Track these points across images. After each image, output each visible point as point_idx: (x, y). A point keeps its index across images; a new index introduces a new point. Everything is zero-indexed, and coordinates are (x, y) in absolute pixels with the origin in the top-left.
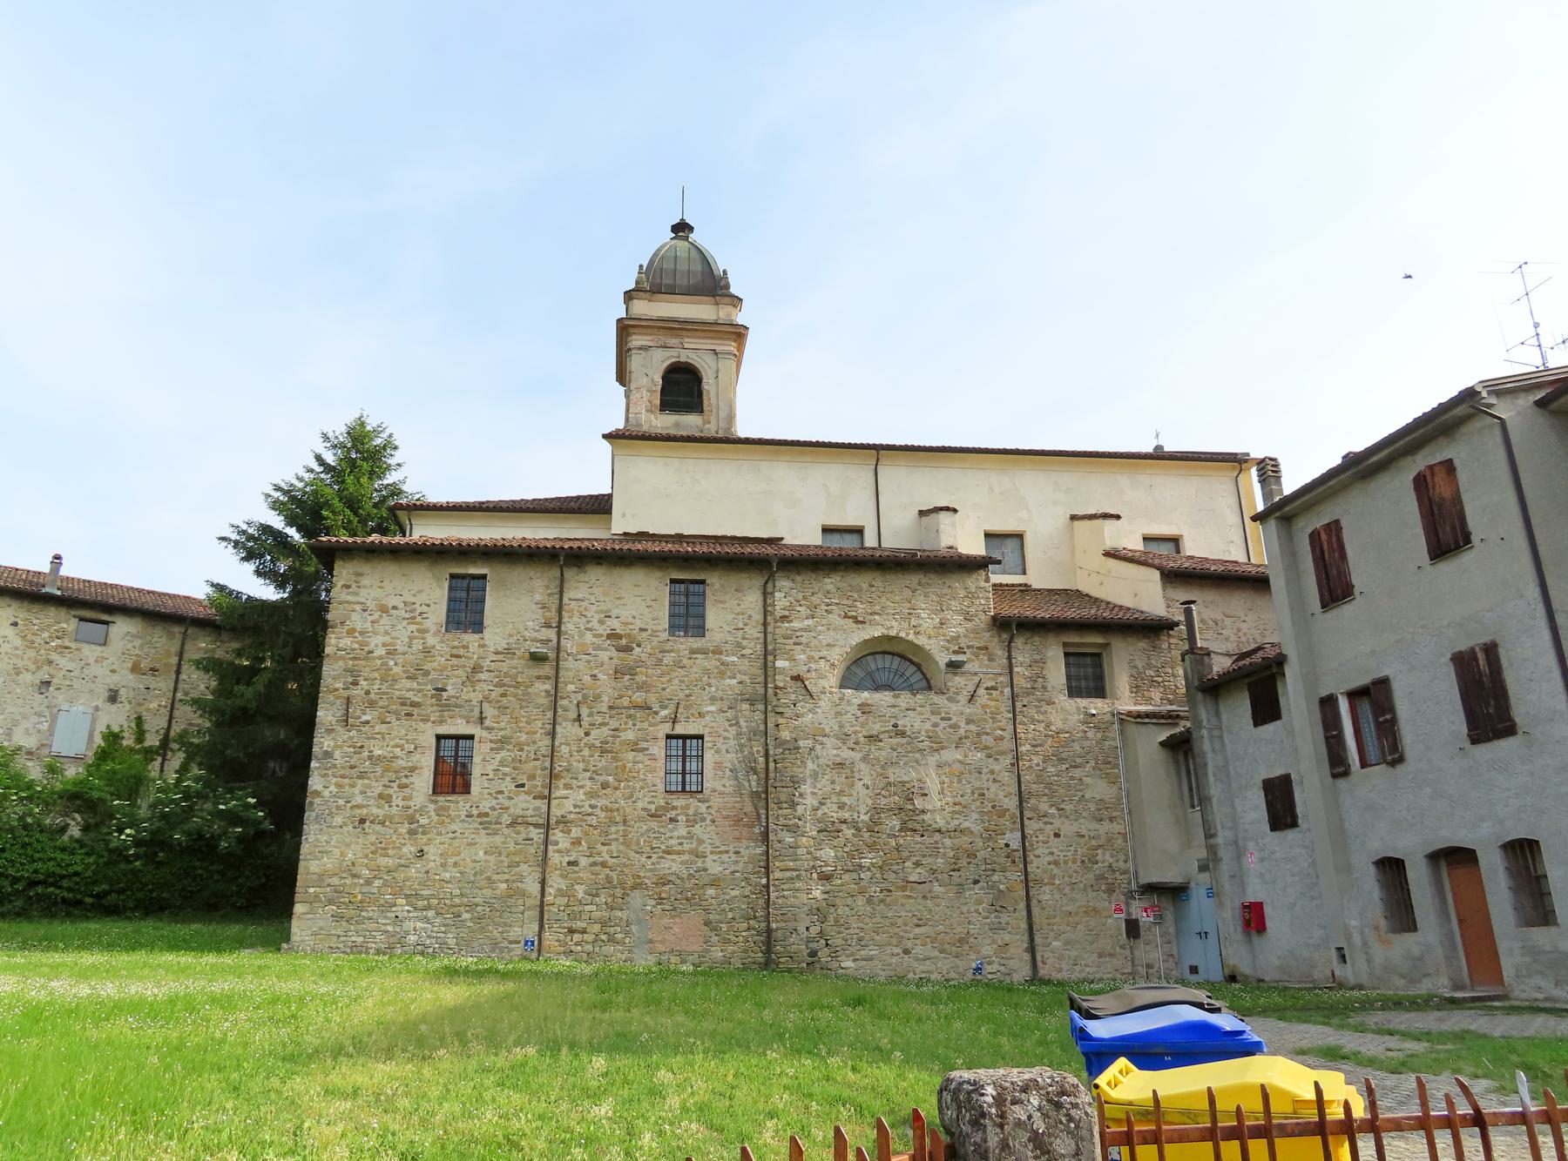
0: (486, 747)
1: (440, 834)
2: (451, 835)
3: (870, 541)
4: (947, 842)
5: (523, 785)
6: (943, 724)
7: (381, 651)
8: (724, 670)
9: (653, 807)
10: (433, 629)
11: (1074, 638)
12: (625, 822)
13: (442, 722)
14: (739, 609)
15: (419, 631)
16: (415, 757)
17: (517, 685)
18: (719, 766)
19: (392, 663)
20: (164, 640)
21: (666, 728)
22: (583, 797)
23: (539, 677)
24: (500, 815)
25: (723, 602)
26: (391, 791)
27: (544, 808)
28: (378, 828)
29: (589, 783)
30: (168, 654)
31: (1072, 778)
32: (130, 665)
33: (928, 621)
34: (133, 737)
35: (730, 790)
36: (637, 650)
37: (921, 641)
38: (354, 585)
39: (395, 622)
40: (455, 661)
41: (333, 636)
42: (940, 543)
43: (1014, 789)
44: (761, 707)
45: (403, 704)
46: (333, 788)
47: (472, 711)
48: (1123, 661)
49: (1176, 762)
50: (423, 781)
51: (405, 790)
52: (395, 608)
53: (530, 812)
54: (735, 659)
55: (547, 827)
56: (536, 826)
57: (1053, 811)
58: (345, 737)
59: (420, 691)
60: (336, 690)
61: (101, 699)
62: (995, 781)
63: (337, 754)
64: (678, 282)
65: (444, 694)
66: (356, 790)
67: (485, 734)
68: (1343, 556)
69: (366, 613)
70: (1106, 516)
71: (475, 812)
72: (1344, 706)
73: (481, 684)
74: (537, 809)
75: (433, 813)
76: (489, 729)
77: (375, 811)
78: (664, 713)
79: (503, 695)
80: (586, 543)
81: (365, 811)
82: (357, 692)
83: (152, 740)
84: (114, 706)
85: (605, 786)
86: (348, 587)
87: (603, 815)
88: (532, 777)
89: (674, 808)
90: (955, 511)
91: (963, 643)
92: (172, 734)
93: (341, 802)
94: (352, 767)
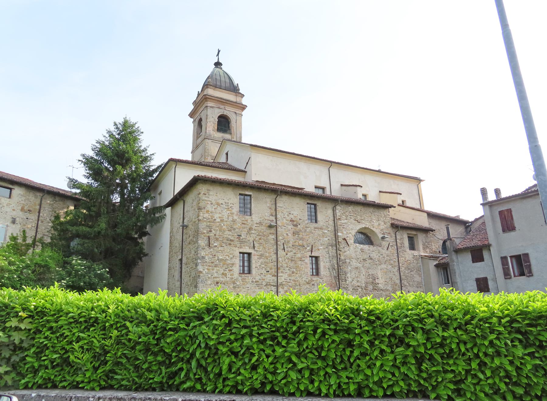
0: (256, 257)
1: (243, 288)
2: (247, 289)
3: (328, 193)
4: (384, 293)
5: (268, 271)
6: (381, 256)
7: (218, 220)
8: (324, 235)
9: (307, 280)
10: (235, 213)
11: (409, 232)
12: (300, 285)
13: (241, 248)
14: (326, 215)
15: (231, 213)
16: (234, 260)
17: (264, 236)
18: (325, 267)
19: (222, 225)
20: (33, 198)
21: (309, 254)
22: (287, 276)
23: (270, 233)
24: (262, 282)
25: (322, 212)
26: (226, 272)
27: (276, 279)
28: (223, 285)
29: (288, 271)
30: (35, 205)
31: (411, 275)
32: (20, 208)
33: (376, 224)
34: (22, 239)
35: (328, 275)
36: (299, 226)
37: (374, 230)
38: (207, 194)
39: (222, 209)
40: (243, 225)
41: (201, 212)
42: (357, 196)
43: (399, 277)
44: (335, 248)
45: (228, 240)
46: (206, 270)
47: (250, 244)
48: (421, 239)
49: (438, 271)
50: (237, 269)
51: (231, 272)
52: (222, 204)
53: (271, 281)
54: (326, 231)
55: (277, 286)
56: (274, 286)
57: (407, 284)
58: (209, 251)
59: (233, 236)
60: (204, 233)
61: (9, 222)
62: (394, 275)
63: (207, 258)
64: (222, 85)
65: (241, 237)
66: (215, 271)
67: (255, 253)
68: (512, 218)
69: (212, 205)
70: (398, 193)
71: (254, 281)
72: (509, 259)
73: (253, 235)
74: (273, 280)
75: (240, 281)
76: (256, 251)
77: (222, 279)
78: (308, 248)
79: (260, 239)
80: (283, 187)
81: (218, 279)
82: (211, 234)
83: (29, 241)
84: (14, 225)
85: (293, 272)
86: (205, 194)
87: (293, 282)
88: (271, 269)
89: (313, 281)
90: (362, 187)
91: (385, 231)
92: (37, 238)
93: (210, 276)
94: (212, 263)
